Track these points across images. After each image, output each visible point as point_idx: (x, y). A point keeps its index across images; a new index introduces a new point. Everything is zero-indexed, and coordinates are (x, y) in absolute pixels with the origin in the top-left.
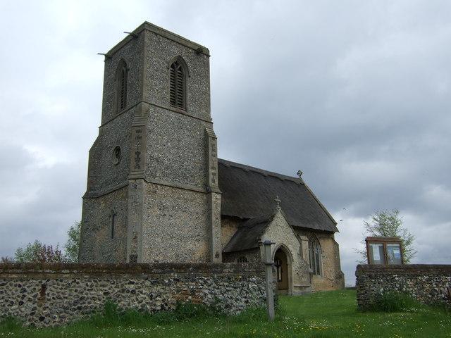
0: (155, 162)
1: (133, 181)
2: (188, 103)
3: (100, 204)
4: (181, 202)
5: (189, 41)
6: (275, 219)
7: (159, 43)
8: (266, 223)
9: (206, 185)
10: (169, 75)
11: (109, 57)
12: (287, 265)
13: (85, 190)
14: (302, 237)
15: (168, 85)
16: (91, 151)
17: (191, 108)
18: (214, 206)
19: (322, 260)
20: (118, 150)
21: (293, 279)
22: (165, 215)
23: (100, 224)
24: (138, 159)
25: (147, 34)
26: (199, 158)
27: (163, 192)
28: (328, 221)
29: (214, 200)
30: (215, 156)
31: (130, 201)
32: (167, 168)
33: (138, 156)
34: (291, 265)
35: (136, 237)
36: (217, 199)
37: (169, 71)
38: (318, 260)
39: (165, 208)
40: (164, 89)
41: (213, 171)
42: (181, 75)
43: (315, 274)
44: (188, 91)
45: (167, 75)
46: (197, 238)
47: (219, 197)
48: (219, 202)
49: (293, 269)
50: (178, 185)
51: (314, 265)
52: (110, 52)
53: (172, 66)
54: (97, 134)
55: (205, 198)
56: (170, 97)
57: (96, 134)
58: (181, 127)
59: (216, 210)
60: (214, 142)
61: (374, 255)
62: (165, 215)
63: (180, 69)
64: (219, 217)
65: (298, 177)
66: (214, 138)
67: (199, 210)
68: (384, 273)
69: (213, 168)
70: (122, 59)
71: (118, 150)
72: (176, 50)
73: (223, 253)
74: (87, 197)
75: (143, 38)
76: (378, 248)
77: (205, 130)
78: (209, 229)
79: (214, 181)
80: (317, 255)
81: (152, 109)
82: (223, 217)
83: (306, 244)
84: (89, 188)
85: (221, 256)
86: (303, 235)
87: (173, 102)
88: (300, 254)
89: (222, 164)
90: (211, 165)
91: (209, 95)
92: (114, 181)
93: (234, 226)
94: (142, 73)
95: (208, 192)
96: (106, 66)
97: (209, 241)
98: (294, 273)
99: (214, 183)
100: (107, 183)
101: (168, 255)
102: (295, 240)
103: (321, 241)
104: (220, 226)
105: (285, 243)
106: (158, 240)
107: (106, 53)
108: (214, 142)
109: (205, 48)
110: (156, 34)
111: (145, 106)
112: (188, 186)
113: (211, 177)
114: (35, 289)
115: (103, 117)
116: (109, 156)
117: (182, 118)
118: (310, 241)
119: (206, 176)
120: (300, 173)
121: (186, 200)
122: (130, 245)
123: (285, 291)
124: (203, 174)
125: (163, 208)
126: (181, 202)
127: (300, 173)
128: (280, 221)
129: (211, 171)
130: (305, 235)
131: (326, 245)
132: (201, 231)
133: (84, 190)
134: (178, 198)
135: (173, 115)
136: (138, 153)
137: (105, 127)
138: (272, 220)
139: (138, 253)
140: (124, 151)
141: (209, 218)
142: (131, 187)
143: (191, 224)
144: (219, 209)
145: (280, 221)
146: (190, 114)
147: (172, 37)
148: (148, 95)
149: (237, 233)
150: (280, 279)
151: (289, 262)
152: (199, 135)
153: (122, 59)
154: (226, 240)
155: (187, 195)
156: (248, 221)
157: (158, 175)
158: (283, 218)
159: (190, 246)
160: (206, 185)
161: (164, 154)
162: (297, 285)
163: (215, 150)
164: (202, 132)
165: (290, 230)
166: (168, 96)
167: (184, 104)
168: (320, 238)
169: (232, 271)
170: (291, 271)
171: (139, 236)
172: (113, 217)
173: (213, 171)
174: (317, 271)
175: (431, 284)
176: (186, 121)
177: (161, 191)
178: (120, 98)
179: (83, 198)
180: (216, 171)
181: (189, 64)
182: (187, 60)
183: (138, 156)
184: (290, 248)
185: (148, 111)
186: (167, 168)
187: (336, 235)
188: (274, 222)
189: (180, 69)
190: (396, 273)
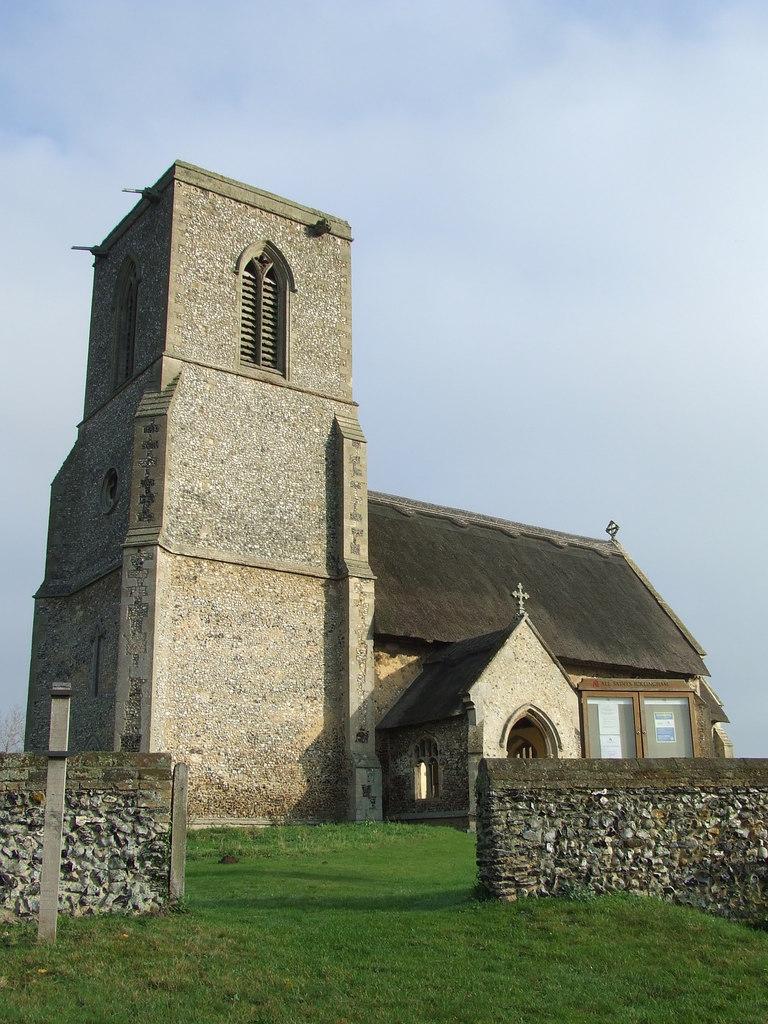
1: (134, 551)
4: (265, 605)
6: (510, 642)
7: (213, 211)
9: (335, 559)
11: (101, 254)
15: (238, 312)
16: (57, 485)
23: (73, 662)
25: (181, 191)
26: (318, 490)
28: (680, 648)
29: (353, 596)
32: (230, 520)
41: (355, 524)
45: (236, 288)
47: (370, 588)
48: (370, 601)
50: (259, 560)
52: (105, 242)
58: (271, 417)
60: (357, 452)
61: (604, 740)
65: (608, 537)
68: (562, 785)
69: (353, 517)
73: (378, 731)
74: (45, 596)
76: (616, 714)
77: (335, 422)
79: (356, 550)
85: (372, 738)
87: (253, 355)
99: (357, 551)
101: (229, 736)
105: (538, 703)
112: (289, 563)
115: (87, 399)
120: (612, 529)
125: (215, 617)
127: (612, 529)
128: (524, 650)
129: (349, 524)
132: (318, 673)
133: (38, 578)
135: (247, 385)
136: (147, 483)
137: (90, 426)
139: (141, 732)
142: (129, 566)
143: (294, 655)
144: (369, 620)
145: (524, 650)
146: (294, 383)
148: (179, 339)
152: (320, 435)
153: (128, 257)
155: (285, 585)
157: (203, 535)
160: (335, 559)
164: (327, 430)
165: (555, 671)
166: (237, 342)
169: (25, 775)
171: (144, 688)
172: (99, 640)
173: (355, 524)
175: (726, 817)
177: (209, 577)
180: (364, 525)
184: (555, 716)
190: (605, 782)
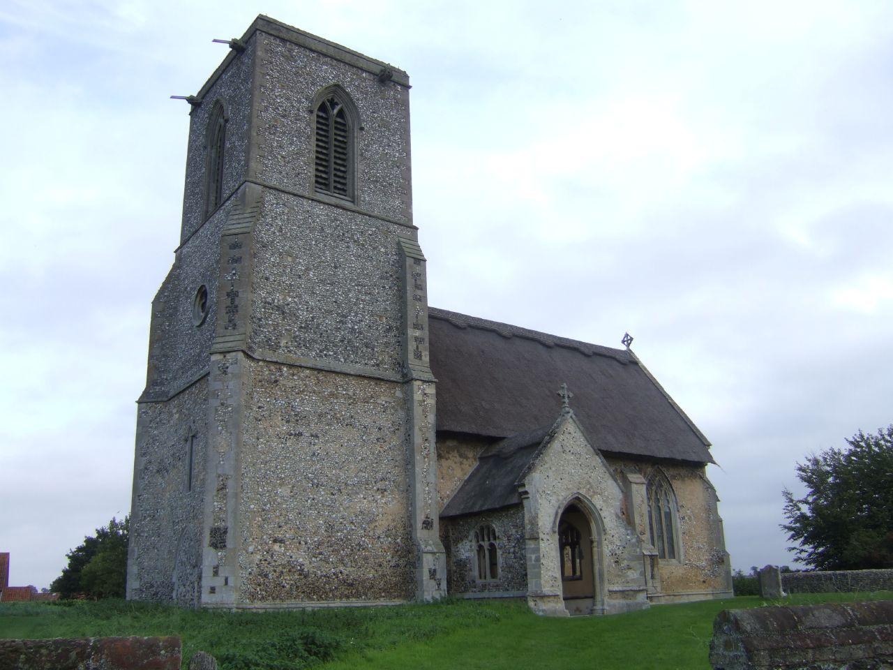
0: (276, 316)
2: (358, 184)
3: (171, 415)
5: (360, 56)
6: (560, 437)
7: (290, 58)
8: (536, 447)
9: (401, 365)
10: (314, 125)
12: (592, 542)
13: (142, 385)
14: (634, 477)
16: (156, 303)
17: (367, 196)
18: (417, 411)
19: (679, 525)
20: (203, 293)
21: (606, 575)
22: (300, 434)
24: (233, 309)
26: (385, 301)
27: (296, 381)
29: (418, 396)
30: (423, 299)
31: (214, 403)
32: (306, 328)
33: (233, 301)
34: (600, 543)
35: (223, 487)
36: (425, 394)
37: (314, 117)
38: (670, 526)
39: (299, 418)
40: (299, 154)
41: (418, 333)
42: (342, 127)
43: (663, 557)
44: (358, 158)
45: (308, 125)
46: (379, 485)
48: (431, 401)
49: (606, 550)
51: (661, 537)
53: (323, 108)
54: (172, 260)
55: (399, 393)
56: (314, 172)
57: (167, 262)
59: (426, 422)
62: (300, 434)
63: (341, 114)
64: (432, 436)
65: (623, 348)
66: (420, 261)
67: (385, 421)
69: (416, 326)
70: (217, 101)
71: (203, 293)
72: (328, 74)
73: (442, 518)
74: (146, 400)
75: (254, 52)
77: (398, 243)
78: (408, 464)
80: (668, 515)
81: (270, 197)
82: (442, 436)
83: (639, 492)
84: (151, 382)
86: (632, 472)
87: (322, 182)
88: (627, 515)
89: (441, 319)
90: (411, 320)
91: (409, 169)
92: (196, 363)
93: (470, 455)
94: (250, 122)
95: (407, 381)
96: (192, 123)
97: (408, 492)
98: (608, 561)
100: (184, 369)
102: (611, 489)
103: (676, 484)
104: (433, 455)
105: (583, 492)
106: (284, 491)
107: (194, 93)
108: (418, 269)
109: (399, 71)
110: (283, 40)
111: (253, 190)
112: (357, 368)
113: (412, 346)
114: (282, 572)
116: (188, 311)
117: (344, 217)
118: (649, 485)
119: (402, 344)
120: (628, 340)
121: (352, 400)
122: (212, 504)
123: (588, 602)
124: (393, 340)
126: (340, 406)
127: (628, 340)
129: (412, 333)
130: (640, 471)
131: (686, 493)
134: (332, 395)
135: (319, 210)
136: (233, 295)
138: (552, 437)
140: (212, 296)
141: (408, 439)
144: (432, 418)
146: (363, 208)
147: (320, 47)
149: (477, 470)
150: (578, 573)
151: (595, 536)
152: (385, 253)
154: (450, 488)
156: (502, 444)
157: (283, 343)
158: (578, 435)
159: (362, 502)
161: (300, 296)
162: (616, 588)
163: (421, 286)
165: (598, 461)
166: (310, 172)
167: (349, 187)
168: (674, 477)
170: (601, 554)
173: (418, 333)
174: (670, 550)
176: (356, 225)
177: (288, 379)
178: (213, 186)
179: (139, 402)
180: (424, 333)
181: (360, 104)
182: (356, 95)
183: (233, 301)
184: (598, 502)
185: (261, 202)
186: (306, 328)
187: (709, 470)
188: (556, 445)
189: (341, 114)
